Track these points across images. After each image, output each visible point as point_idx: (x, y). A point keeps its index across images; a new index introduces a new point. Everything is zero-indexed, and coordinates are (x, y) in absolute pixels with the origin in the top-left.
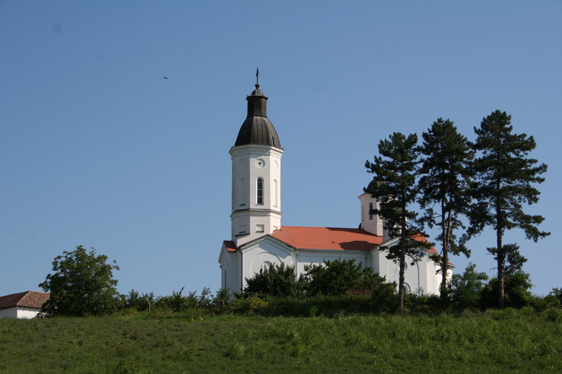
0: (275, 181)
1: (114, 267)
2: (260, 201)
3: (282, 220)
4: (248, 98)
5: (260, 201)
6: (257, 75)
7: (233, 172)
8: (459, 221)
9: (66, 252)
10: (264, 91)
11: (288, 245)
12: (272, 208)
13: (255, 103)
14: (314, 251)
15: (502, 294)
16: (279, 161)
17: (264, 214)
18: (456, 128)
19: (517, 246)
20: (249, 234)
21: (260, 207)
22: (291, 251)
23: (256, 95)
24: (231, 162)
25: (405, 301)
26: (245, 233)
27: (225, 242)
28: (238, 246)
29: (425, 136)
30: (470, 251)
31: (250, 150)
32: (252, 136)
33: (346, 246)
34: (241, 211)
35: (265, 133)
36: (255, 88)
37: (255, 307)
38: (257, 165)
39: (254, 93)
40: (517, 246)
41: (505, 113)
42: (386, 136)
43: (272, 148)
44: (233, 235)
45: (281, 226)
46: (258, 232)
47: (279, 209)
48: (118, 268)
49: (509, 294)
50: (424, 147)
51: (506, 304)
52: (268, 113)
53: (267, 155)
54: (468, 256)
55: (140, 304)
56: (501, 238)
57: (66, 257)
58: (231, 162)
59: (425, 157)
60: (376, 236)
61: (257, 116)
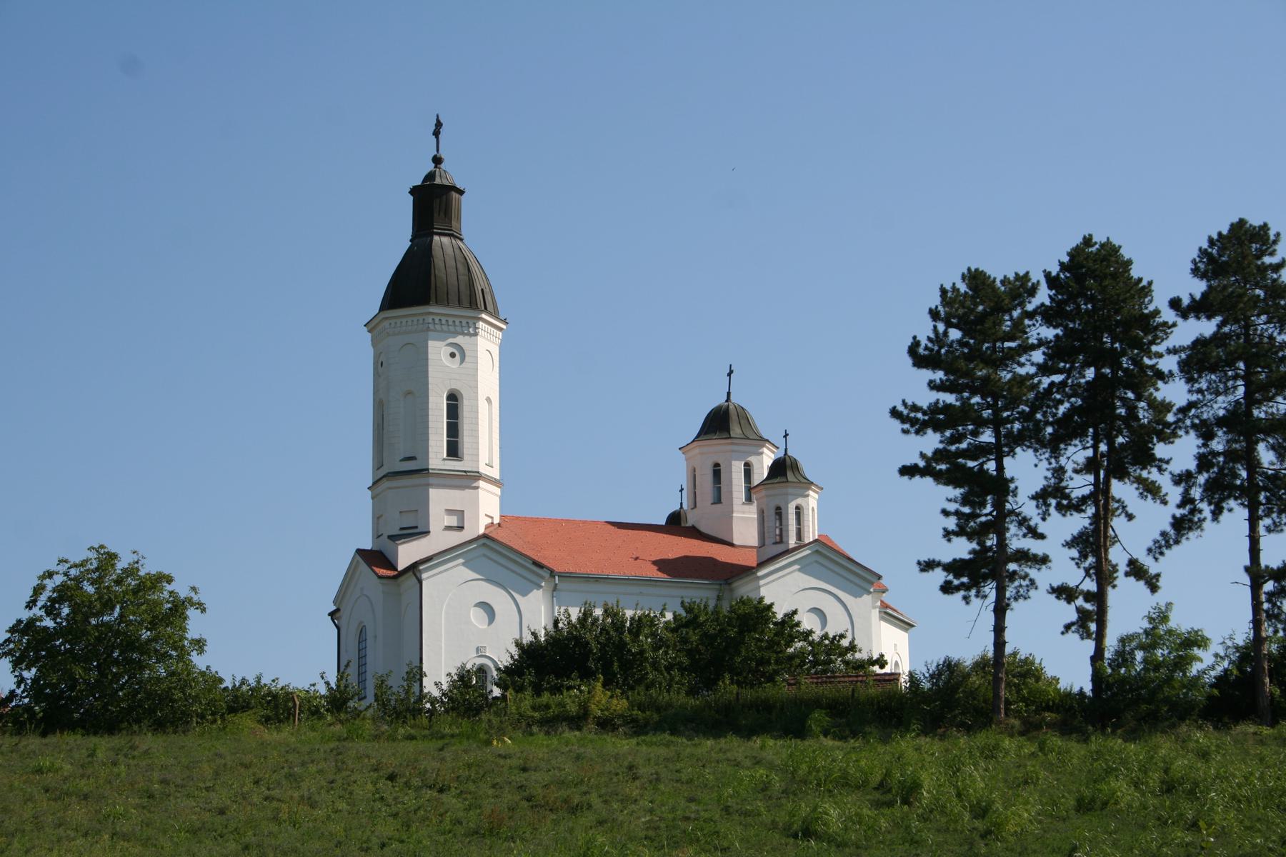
0: (489, 400)
2: (453, 450)
3: (501, 498)
4: (414, 191)
5: (453, 450)
6: (436, 133)
7: (377, 375)
8: (1118, 501)
9: (66, 561)
10: (453, 173)
11: (536, 563)
12: (483, 469)
13: (433, 203)
14: (597, 580)
15: (1264, 684)
17: (465, 482)
20: (428, 532)
21: (453, 465)
22: (542, 578)
23: (438, 181)
24: (369, 353)
25: (1008, 703)
26: (416, 531)
27: (359, 551)
28: (402, 564)
29: (1052, 281)
30: (1158, 575)
31: (430, 319)
32: (426, 285)
33: (674, 568)
34: (402, 474)
35: (464, 278)
36: (431, 166)
37: (599, 713)
38: (446, 360)
39: (430, 176)
41: (1265, 227)
42: (954, 278)
43: (484, 316)
44: (377, 536)
46: (448, 528)
47: (495, 473)
49: (1280, 685)
50: (1267, 260)
52: (465, 233)
53: (471, 335)
54: (1154, 588)
56: (1035, 556)
57: (66, 574)
58: (371, 350)
59: (1049, 333)
60: (732, 545)
61: (440, 234)
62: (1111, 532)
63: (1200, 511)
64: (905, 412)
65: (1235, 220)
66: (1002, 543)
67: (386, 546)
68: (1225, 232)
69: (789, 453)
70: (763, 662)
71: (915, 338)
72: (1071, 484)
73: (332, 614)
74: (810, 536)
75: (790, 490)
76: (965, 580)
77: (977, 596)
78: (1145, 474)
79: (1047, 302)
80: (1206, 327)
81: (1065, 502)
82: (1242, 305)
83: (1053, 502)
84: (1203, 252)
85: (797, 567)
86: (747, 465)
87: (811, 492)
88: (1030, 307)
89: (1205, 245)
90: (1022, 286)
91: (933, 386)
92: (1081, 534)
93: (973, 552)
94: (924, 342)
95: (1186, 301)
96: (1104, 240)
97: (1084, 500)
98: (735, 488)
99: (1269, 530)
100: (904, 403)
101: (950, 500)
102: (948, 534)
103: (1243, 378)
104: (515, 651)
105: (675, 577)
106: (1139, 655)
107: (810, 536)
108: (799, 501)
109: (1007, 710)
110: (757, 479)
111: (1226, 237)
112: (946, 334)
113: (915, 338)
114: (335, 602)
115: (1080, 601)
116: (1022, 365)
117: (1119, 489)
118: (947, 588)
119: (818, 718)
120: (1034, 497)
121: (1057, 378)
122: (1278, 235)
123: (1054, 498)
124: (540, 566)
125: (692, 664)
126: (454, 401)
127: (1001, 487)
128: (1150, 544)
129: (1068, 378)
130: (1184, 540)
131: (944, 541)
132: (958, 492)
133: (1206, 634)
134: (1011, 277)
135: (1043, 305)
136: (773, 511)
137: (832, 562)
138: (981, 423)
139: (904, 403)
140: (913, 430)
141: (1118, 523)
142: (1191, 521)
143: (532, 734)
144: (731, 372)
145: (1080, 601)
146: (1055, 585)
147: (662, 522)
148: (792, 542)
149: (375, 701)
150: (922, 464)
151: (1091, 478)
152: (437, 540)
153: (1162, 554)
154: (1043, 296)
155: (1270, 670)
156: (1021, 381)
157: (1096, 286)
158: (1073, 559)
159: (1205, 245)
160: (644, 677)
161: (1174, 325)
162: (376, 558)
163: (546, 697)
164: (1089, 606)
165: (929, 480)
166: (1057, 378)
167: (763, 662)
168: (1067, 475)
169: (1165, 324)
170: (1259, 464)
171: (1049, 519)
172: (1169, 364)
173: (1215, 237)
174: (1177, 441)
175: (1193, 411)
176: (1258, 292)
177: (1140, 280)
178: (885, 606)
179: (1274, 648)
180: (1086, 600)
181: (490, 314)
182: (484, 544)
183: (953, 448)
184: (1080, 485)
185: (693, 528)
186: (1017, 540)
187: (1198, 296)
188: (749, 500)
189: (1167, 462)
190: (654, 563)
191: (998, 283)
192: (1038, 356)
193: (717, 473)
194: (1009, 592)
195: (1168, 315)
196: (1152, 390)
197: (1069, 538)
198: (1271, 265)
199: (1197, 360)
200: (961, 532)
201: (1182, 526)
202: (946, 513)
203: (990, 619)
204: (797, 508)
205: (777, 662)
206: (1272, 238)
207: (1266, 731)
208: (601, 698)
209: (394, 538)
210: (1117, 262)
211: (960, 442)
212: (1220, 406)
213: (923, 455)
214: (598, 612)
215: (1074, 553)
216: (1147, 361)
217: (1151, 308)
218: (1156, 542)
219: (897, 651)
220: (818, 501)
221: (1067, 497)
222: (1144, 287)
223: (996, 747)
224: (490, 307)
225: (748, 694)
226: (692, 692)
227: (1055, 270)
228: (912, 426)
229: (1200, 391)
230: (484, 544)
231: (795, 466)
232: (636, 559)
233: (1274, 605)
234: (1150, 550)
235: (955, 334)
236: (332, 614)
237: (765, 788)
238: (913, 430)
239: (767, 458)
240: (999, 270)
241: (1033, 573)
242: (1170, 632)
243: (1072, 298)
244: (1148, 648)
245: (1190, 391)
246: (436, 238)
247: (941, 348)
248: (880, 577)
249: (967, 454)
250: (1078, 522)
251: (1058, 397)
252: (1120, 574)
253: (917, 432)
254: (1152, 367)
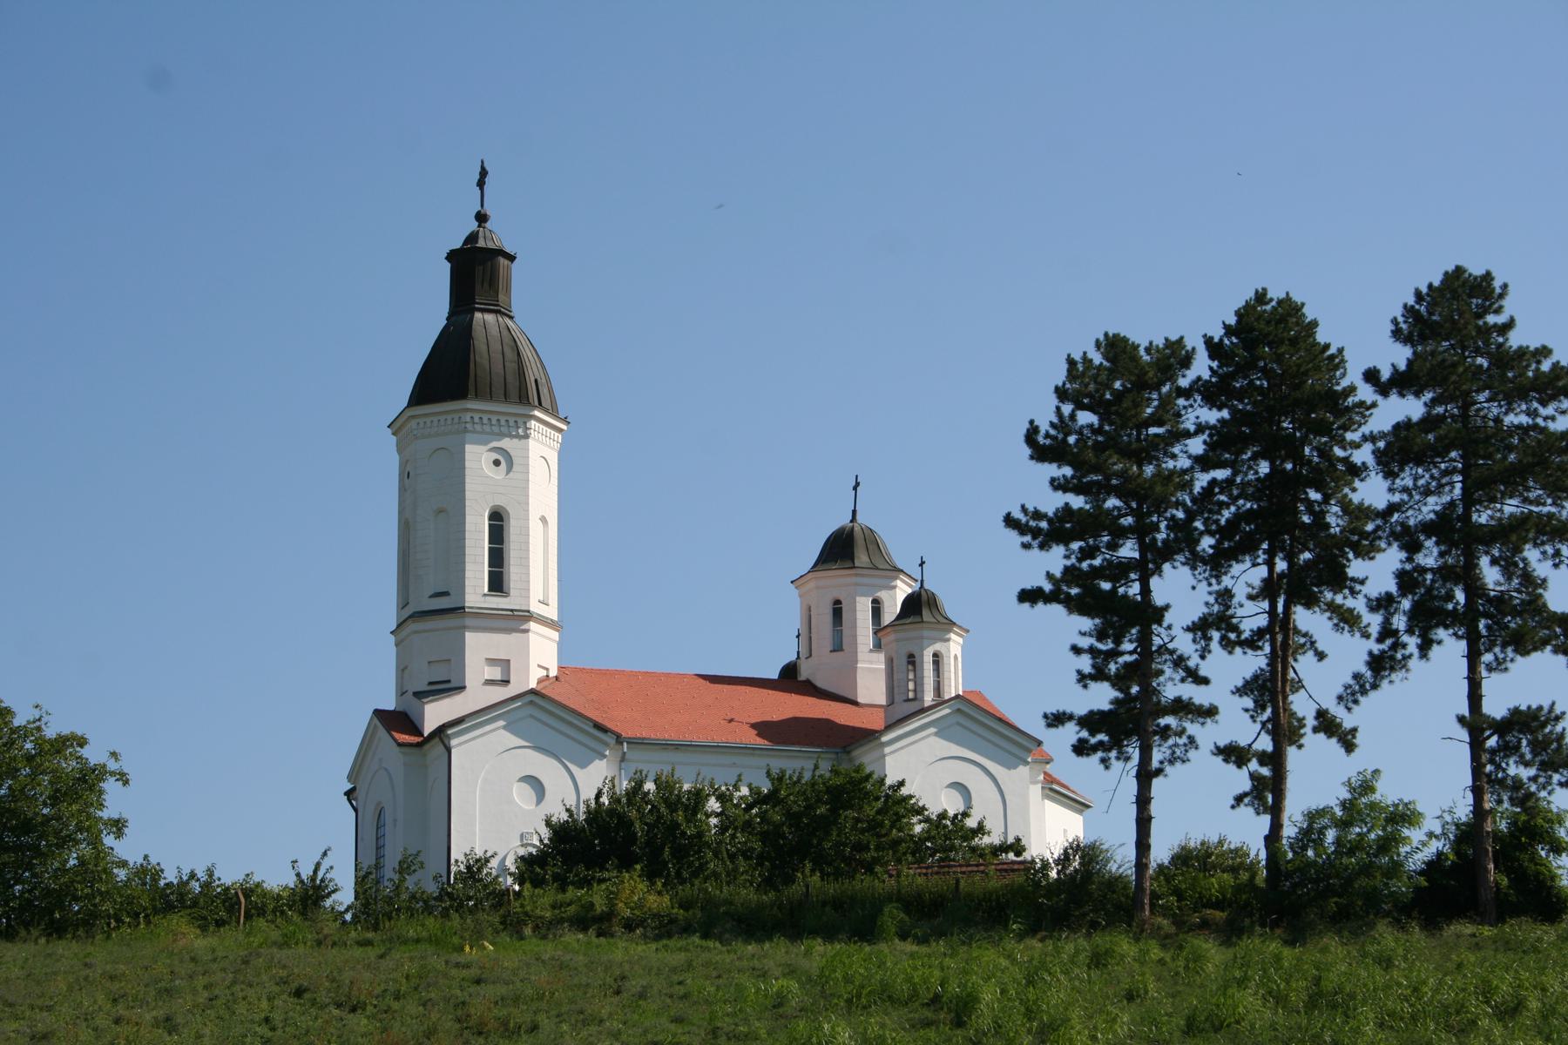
0: (543, 520)
1: (112, 774)
2: (497, 584)
3: (561, 645)
4: (452, 256)
5: (497, 584)
6: (481, 184)
7: (403, 489)
10: (501, 234)
11: (599, 727)
12: (535, 608)
13: (476, 271)
14: (677, 747)
15: (1487, 871)
16: (553, 458)
17: (512, 624)
18: (1314, 324)
19: (1558, 710)
21: (497, 602)
22: (606, 744)
23: (481, 243)
24: (394, 460)
25: (1155, 896)
26: (448, 687)
27: (378, 713)
28: (429, 727)
29: (1214, 349)
30: (1354, 730)
31: (467, 417)
32: (466, 375)
33: (775, 732)
34: (432, 615)
36: (474, 225)
37: (628, 913)
38: (489, 470)
39: (472, 238)
40: (1558, 710)
41: (1488, 276)
42: (1085, 346)
43: (537, 413)
44: (401, 693)
45: (560, 668)
46: (490, 682)
47: (552, 612)
48: (123, 778)
50: (1491, 319)
51: (1502, 911)
53: (518, 437)
54: (1349, 747)
55: (161, 900)
56: (1479, 685)
58: (397, 457)
59: (1211, 416)
60: (855, 703)
62: (1291, 674)
63: (1404, 646)
64: (1024, 520)
65: (1451, 268)
66: (1149, 692)
67: (411, 704)
68: (1436, 283)
69: (926, 586)
70: (861, 847)
71: (1031, 422)
72: (1240, 612)
73: (349, 794)
74: (951, 691)
75: (926, 633)
76: (1102, 737)
77: (1118, 758)
78: (1339, 599)
79: (1206, 375)
80: (1411, 408)
81: (1232, 636)
82: (1454, 378)
83: (1216, 635)
84: (1409, 311)
85: (932, 730)
86: (876, 602)
87: (953, 636)
88: (1184, 383)
89: (1411, 301)
90: (1173, 353)
91: (1058, 485)
92: (1256, 677)
93: (1115, 701)
94: (1044, 427)
95: (1386, 374)
96: (1282, 296)
97: (1260, 633)
98: (860, 631)
99: (1490, 669)
100: (1024, 509)
101: (1084, 634)
102: (1083, 678)
103: (1461, 472)
104: (546, 833)
105: (778, 743)
106: (1331, 835)
107: (951, 691)
108: (938, 647)
109: (1152, 906)
110: (889, 616)
111: (1439, 289)
112: (1073, 417)
113: (1031, 422)
114: (349, 778)
115: (1254, 765)
116: (1174, 456)
117: (1304, 618)
118: (1081, 749)
119: (892, 916)
120: (1188, 629)
121: (1221, 474)
122: (1505, 286)
123: (1218, 629)
124: (604, 730)
125: (781, 848)
126: (498, 521)
127: (1148, 614)
128: (1340, 690)
129: (1235, 474)
130: (1385, 684)
131: (1078, 687)
132: (1087, 623)
133: (1420, 808)
134: (1160, 342)
135: (1199, 378)
136: (904, 660)
137: (982, 726)
138: (1119, 534)
139: (1024, 509)
140: (1035, 543)
141: (1304, 665)
142: (1392, 658)
143: (522, 938)
144: (857, 484)
145: (1254, 765)
146: (1222, 744)
147: (775, 675)
148: (929, 698)
149: (411, 898)
150: (1048, 587)
151: (1265, 605)
152: (475, 696)
153: (1356, 702)
154: (1202, 367)
155: (1495, 852)
156: (1168, 478)
157: (1271, 352)
158: (1247, 710)
159: (1411, 301)
160: (702, 867)
161: (1374, 405)
162: (398, 721)
163: (572, 893)
164: (1265, 771)
165: (1057, 610)
166: (1221, 474)
167: (861, 847)
168: (1235, 601)
169: (1362, 404)
170: (1483, 588)
171: (1209, 657)
172: (1363, 455)
173: (1424, 290)
174: (1379, 556)
175: (1396, 516)
176: (1479, 360)
177: (1327, 346)
178: (1049, 780)
179: (1503, 826)
180: (1262, 764)
181: (546, 411)
182: (531, 702)
183: (1085, 565)
184: (1252, 616)
185: (808, 682)
186: (1172, 687)
187: (1402, 366)
188: (878, 646)
189: (1362, 582)
190: (754, 726)
191: (1142, 352)
192: (1197, 446)
193: (837, 611)
194: (1157, 756)
195: (1366, 393)
196: (1346, 490)
197: (1240, 683)
198: (1495, 325)
199: (1400, 450)
200: (1099, 675)
201: (1381, 665)
202: (1076, 650)
203: (1131, 787)
204: (935, 655)
205: (878, 848)
206: (1498, 291)
207: (1487, 931)
208: (634, 891)
209: (419, 695)
210: (1297, 324)
211: (1093, 558)
212: (1431, 506)
213: (1049, 576)
214: (649, 786)
215: (1248, 702)
216: (1338, 452)
217: (1345, 383)
218: (1347, 687)
219: (1050, 832)
220: (963, 647)
221: (1235, 629)
222: (1332, 357)
223: (1109, 953)
224: (546, 402)
225: (832, 889)
226: (768, 883)
227: (1217, 333)
228: (1034, 538)
229: (1405, 490)
230: (531, 702)
231: (932, 602)
232: (731, 721)
233: (1498, 767)
234: (1340, 698)
235: (1086, 418)
236: (349, 794)
237: (780, 1001)
238: (1035, 543)
239: (902, 590)
240: (1146, 333)
241: (1192, 728)
242: (1373, 806)
243: (1243, 369)
244: (1343, 824)
245: (1391, 490)
246: (478, 315)
247: (1067, 434)
248: (1040, 743)
249: (1097, 573)
250: (1252, 663)
251: (1223, 498)
252: (1308, 730)
253: (1042, 547)
254: (1346, 460)
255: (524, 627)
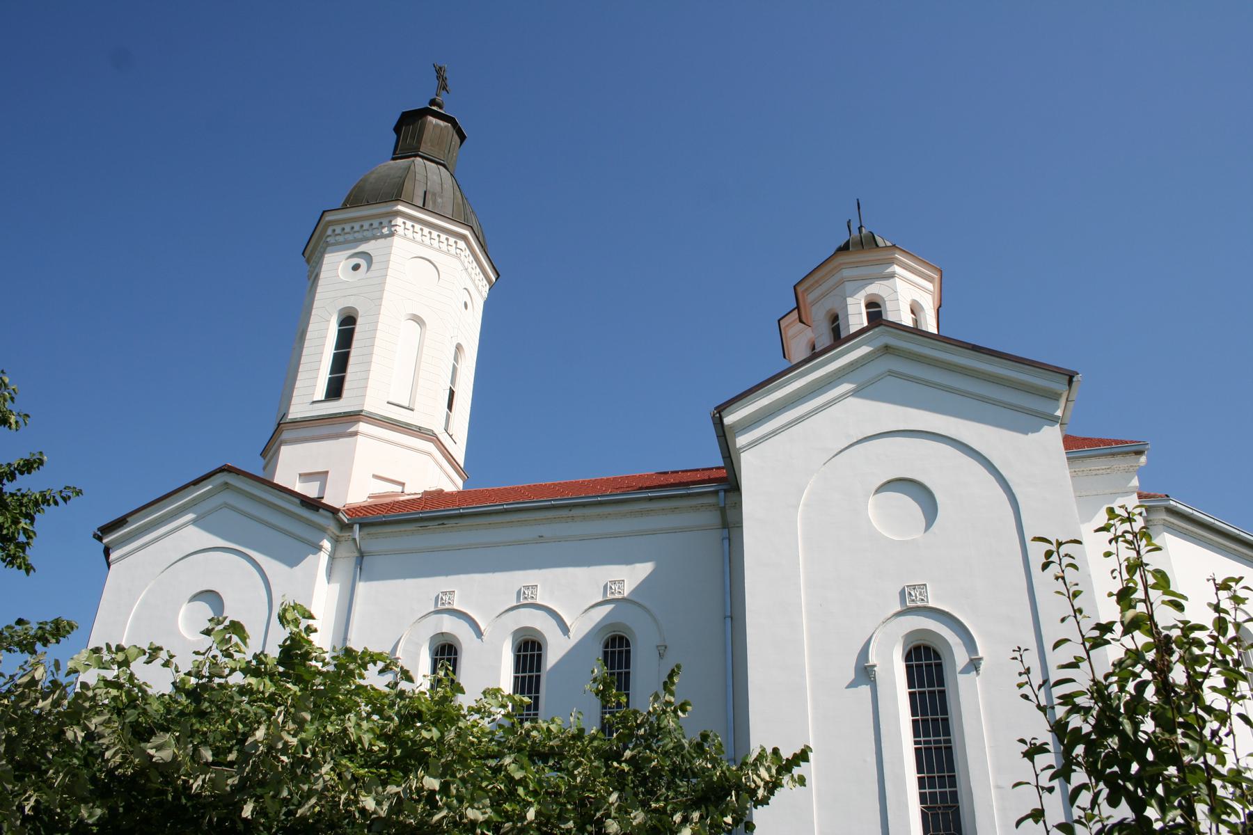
2: (335, 390)
5: (335, 390)
22: (322, 530)
43: (400, 208)
75: (846, 273)
85: (846, 387)
87: (897, 269)
108: (875, 288)
126: (348, 324)
204: (869, 305)
230: (887, 349)
255: (353, 429)
